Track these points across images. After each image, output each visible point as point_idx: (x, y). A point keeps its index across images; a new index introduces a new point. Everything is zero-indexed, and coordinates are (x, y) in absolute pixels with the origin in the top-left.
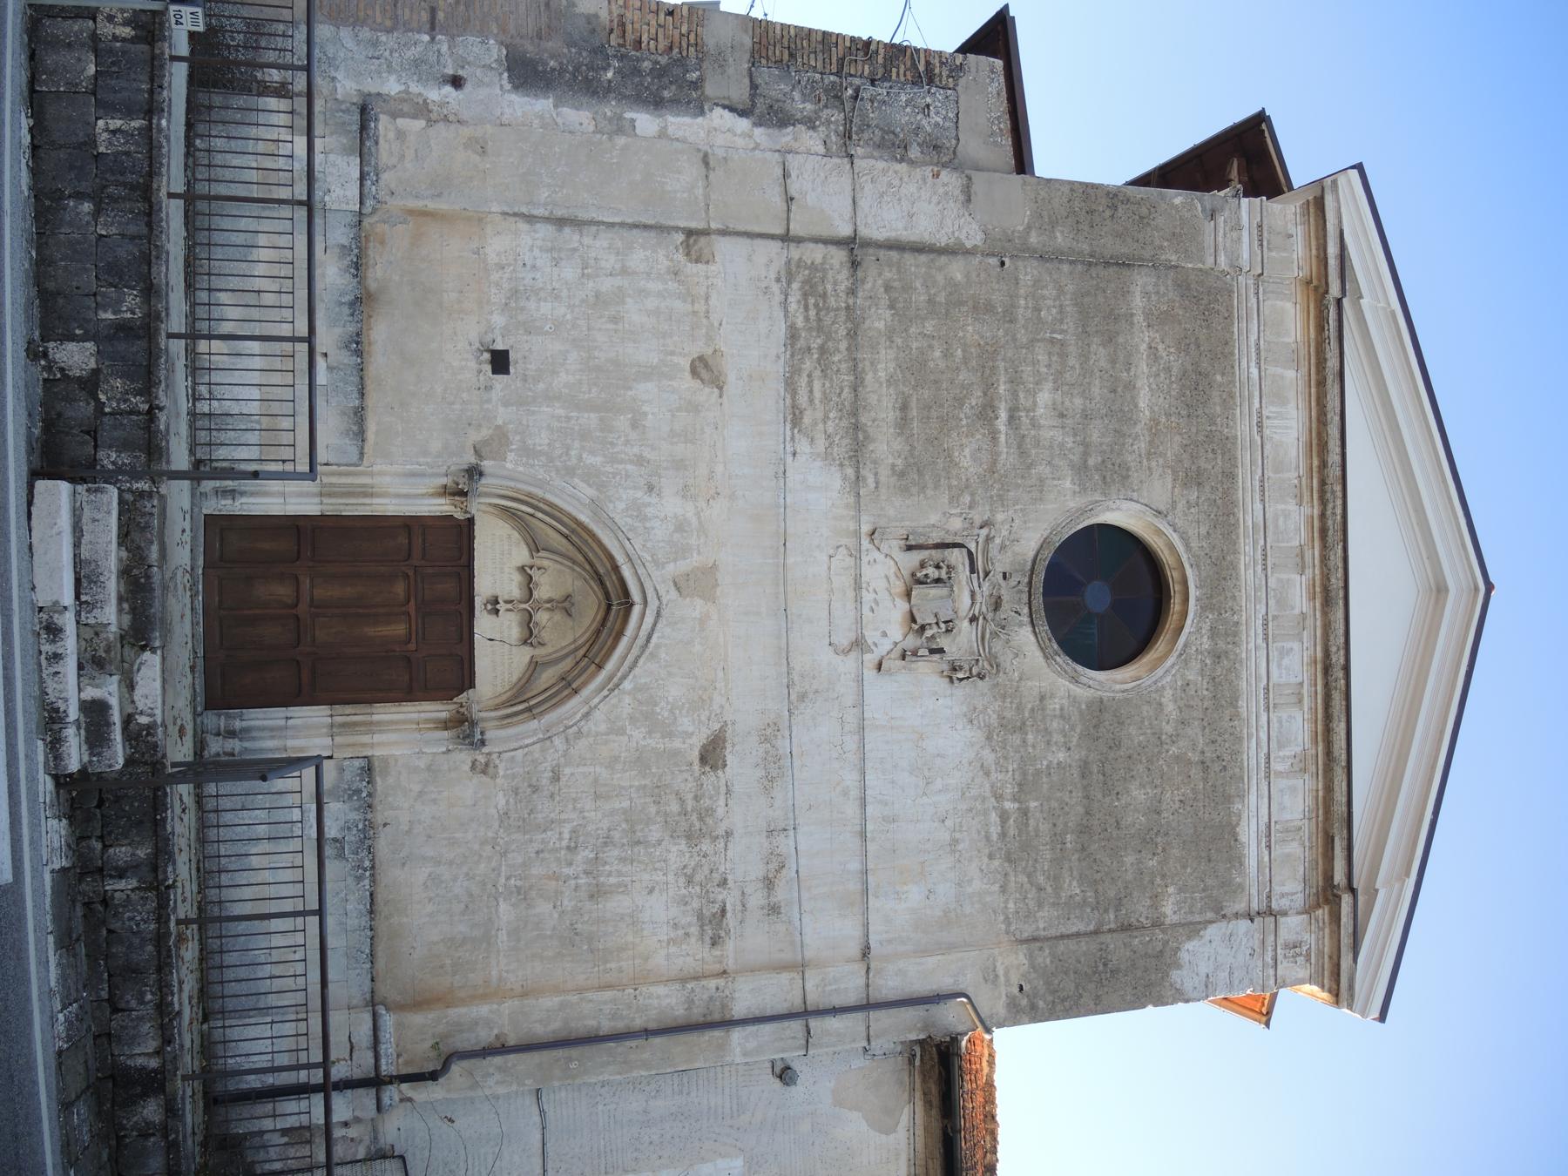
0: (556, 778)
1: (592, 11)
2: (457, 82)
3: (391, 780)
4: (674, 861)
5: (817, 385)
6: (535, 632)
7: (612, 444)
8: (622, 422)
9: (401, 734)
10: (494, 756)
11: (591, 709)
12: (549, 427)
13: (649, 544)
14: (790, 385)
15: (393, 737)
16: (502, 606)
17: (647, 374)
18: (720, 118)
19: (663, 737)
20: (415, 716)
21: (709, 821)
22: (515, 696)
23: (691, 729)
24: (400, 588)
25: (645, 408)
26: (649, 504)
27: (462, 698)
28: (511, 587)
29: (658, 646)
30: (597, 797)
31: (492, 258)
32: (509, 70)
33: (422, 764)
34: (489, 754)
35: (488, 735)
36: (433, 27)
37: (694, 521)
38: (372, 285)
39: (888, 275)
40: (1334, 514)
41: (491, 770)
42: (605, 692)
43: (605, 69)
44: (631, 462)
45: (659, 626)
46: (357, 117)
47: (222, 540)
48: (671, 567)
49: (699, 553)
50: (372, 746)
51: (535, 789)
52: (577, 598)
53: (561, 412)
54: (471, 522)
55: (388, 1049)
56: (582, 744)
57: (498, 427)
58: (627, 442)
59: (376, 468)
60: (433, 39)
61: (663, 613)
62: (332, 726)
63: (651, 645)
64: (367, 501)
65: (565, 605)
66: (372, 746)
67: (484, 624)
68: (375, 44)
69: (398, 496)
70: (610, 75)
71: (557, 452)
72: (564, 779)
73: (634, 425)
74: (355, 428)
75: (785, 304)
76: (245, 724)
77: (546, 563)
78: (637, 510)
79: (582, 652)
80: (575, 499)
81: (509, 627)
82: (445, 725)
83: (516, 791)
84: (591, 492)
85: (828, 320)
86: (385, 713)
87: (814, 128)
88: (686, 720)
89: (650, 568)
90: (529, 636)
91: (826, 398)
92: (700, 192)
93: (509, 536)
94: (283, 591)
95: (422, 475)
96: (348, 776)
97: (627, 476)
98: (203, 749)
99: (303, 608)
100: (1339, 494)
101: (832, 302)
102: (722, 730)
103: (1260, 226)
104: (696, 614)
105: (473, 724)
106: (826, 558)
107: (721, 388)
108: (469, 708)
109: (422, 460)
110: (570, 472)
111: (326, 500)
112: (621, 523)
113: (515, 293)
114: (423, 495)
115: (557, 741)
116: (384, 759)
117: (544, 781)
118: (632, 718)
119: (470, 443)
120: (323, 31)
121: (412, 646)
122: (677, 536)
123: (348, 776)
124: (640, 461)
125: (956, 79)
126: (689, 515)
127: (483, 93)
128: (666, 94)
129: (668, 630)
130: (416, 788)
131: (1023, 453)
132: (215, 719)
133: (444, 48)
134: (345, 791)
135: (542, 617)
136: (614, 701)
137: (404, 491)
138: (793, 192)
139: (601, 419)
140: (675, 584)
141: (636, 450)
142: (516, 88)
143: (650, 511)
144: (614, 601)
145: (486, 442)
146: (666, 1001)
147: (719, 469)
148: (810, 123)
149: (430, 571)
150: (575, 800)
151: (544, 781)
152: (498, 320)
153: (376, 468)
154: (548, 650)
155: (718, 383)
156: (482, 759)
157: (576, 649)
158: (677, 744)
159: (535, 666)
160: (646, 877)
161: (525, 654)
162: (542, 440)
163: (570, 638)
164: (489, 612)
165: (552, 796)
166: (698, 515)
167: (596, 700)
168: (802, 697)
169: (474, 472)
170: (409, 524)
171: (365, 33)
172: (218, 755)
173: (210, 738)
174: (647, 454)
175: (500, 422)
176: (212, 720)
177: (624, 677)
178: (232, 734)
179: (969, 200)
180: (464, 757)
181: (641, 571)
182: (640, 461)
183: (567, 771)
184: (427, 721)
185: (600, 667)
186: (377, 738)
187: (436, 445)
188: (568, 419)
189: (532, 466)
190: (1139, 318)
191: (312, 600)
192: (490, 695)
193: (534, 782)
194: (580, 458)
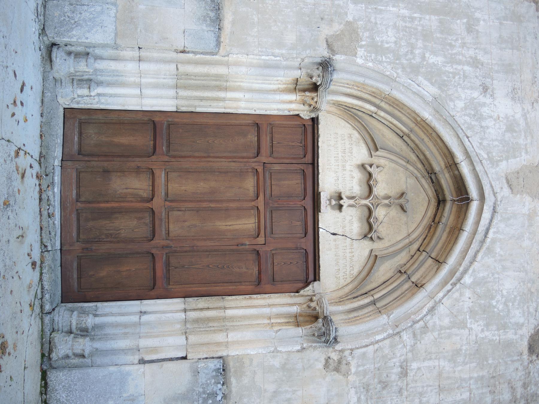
0: (404, 373)
3: (246, 381)
6: (375, 227)
7: (451, 45)
8: (459, 25)
9: (254, 328)
10: (347, 353)
11: (436, 304)
12: (395, 26)
13: (485, 143)
15: (248, 335)
16: (345, 202)
19: (498, 329)
20: (267, 310)
22: (356, 288)
23: (522, 320)
24: (250, 184)
25: (478, 15)
26: (484, 104)
27: (308, 291)
28: (353, 184)
29: (494, 241)
30: (441, 390)
33: (276, 362)
34: (342, 351)
35: (340, 333)
37: (522, 122)
41: (343, 367)
42: (449, 287)
44: (468, 64)
45: (495, 221)
47: (80, 134)
48: (503, 165)
49: (527, 152)
50: (227, 345)
51: (385, 385)
52: (410, 195)
53: (405, 12)
54: (315, 121)
56: (429, 338)
57: (348, 23)
58: (464, 45)
59: (232, 58)
61: (498, 209)
62: (186, 321)
63: (488, 240)
64: (222, 94)
65: (400, 203)
66: (227, 345)
67: (328, 219)
69: (251, 90)
71: (403, 50)
72: (411, 374)
73: (470, 29)
74: (212, 14)
76: (98, 320)
77: (382, 162)
78: (473, 107)
79: (416, 246)
80: (418, 96)
81: (351, 222)
82: (297, 321)
83: (367, 388)
84: (434, 90)
86: (239, 307)
88: (517, 312)
89: (488, 168)
90: (369, 231)
93: (350, 136)
94: (138, 185)
95: (277, 67)
96: (202, 378)
97: (465, 77)
98: (50, 351)
99: (157, 203)
104: (525, 211)
105: (326, 319)
108: (320, 302)
109: (277, 51)
110: (415, 70)
111: (183, 93)
112: (460, 121)
114: (275, 91)
115: (405, 336)
116: (239, 359)
117: (393, 377)
118: (472, 312)
119: (322, 37)
121: (261, 240)
122: (508, 135)
123: (202, 378)
124: (475, 63)
126: (518, 116)
129: (502, 225)
130: (271, 388)
132: (67, 314)
134: (199, 395)
135: (380, 213)
136: (456, 295)
137: (256, 86)
139: (441, 22)
140: (508, 182)
141: (471, 52)
143: (485, 111)
144: (450, 197)
145: (338, 37)
149: (277, 167)
150: (421, 394)
151: (393, 377)
153: (232, 58)
154: (385, 243)
156: (335, 356)
157: (411, 243)
158: (510, 335)
159: (374, 259)
161: (364, 249)
162: (389, 37)
163: (404, 234)
164: (333, 207)
165: (400, 391)
166: (525, 116)
167: (441, 295)
169: (325, 65)
170: (259, 124)
172: (67, 357)
173: (58, 338)
174: (481, 57)
175: (350, 18)
176: (67, 316)
177: (465, 271)
178: (84, 332)
180: (318, 355)
181: (479, 168)
182: (475, 63)
183: (415, 365)
184: (279, 316)
185: (439, 262)
186: (233, 336)
187: (290, 38)
188: (412, 19)
189: (381, 62)
191: (167, 194)
192: (333, 287)
193: (384, 378)
194: (423, 58)
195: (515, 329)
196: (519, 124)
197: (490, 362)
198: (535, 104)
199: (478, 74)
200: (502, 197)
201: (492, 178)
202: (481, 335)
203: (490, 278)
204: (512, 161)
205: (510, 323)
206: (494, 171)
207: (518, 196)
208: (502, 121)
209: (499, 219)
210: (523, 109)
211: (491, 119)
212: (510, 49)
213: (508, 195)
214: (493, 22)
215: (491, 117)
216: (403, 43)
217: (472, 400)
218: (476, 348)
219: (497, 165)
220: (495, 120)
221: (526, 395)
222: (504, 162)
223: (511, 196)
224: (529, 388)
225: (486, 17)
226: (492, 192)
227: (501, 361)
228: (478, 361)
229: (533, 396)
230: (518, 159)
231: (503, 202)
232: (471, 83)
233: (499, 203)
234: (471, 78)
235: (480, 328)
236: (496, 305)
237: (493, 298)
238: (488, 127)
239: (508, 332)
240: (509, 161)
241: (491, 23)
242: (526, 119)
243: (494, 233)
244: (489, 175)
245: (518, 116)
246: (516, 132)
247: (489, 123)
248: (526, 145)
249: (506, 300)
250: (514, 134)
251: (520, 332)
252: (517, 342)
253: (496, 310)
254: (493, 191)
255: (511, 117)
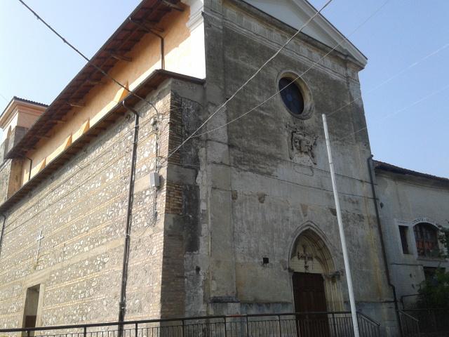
1: (172, 220)
2: (198, 269)
5: (261, 166)
14: (263, 174)
17: (264, 217)
18: (199, 180)
31: (243, 261)
32: (192, 251)
36: (183, 277)
38: (253, 299)
39: (234, 137)
43: (190, 218)
46: (218, 304)
55: (388, 299)
60: (186, 277)
67: (311, 271)
68: (189, 298)
70: (191, 216)
75: (245, 171)
85: (246, 158)
87: (198, 150)
90: (311, 258)
91: (264, 164)
92: (222, 192)
101: (242, 156)
102: (301, 205)
103: (211, 10)
113: (250, 255)
120: (187, 315)
125: (179, 96)
127: (199, 260)
128: (194, 198)
131: (269, 109)
133: (188, 273)
138: (219, 162)
142: (198, 249)
146: (375, 231)
147: (282, 199)
148: (197, 151)
152: (256, 260)
155: (264, 195)
159: (317, 257)
168: (322, 186)
171: (186, 301)
179: (215, 104)
190: (236, 60)
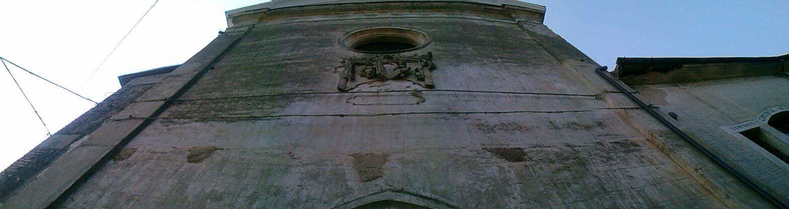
4: (602, 167)
13: (325, 199)
21: (565, 155)
23: (495, 168)
25: (208, 190)
40: (353, 6)
45: (412, 191)
49: (341, 164)
63: (433, 196)
100: (346, 5)
104: (400, 167)
106: (355, 106)
107: (216, 149)
129: (416, 185)
158: (512, 175)
160: (623, 181)
174: (250, 191)
195: (505, 172)
196: (312, 169)
197: (542, 189)
198: (295, 157)
199: (264, 198)
200: (387, 185)
201: (365, 193)
202: (520, 199)
203: (458, 195)
204: (348, 176)
205: (499, 176)
206: (357, 192)
207: (384, 172)
208: (305, 183)
209: (410, 188)
210: (298, 166)
211: (300, 192)
212: (248, 170)
213: (384, 180)
214: (219, 180)
215: (298, 192)
216: (543, 154)
217: (582, 199)
218: (534, 202)
219: (351, 189)
220: (302, 189)
221: (559, 161)
222: (349, 183)
223: (384, 177)
224: (553, 159)
225: (213, 184)
226: (381, 194)
227: (538, 181)
228: (546, 199)
229: (558, 156)
230: (346, 172)
231: (391, 185)
232: (271, 204)
233: (392, 188)
234: (266, 203)
235: (513, 201)
236: (485, 188)
237: (479, 192)
238: (308, 196)
239: (509, 178)
240: (348, 179)
241: (220, 181)
242: (307, 164)
243: (425, 191)
244: (362, 196)
245: (303, 170)
246: (318, 172)
247: (304, 194)
248: (332, 165)
249: (478, 181)
250: (320, 174)
251: (507, 168)
252: (517, 170)
253: (490, 188)
254: (378, 193)
255: (303, 176)
